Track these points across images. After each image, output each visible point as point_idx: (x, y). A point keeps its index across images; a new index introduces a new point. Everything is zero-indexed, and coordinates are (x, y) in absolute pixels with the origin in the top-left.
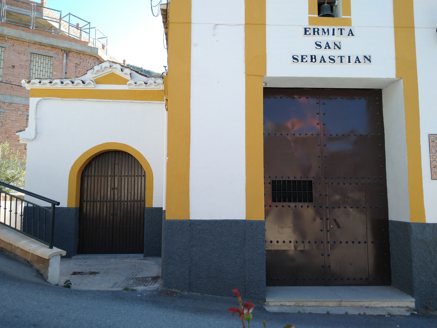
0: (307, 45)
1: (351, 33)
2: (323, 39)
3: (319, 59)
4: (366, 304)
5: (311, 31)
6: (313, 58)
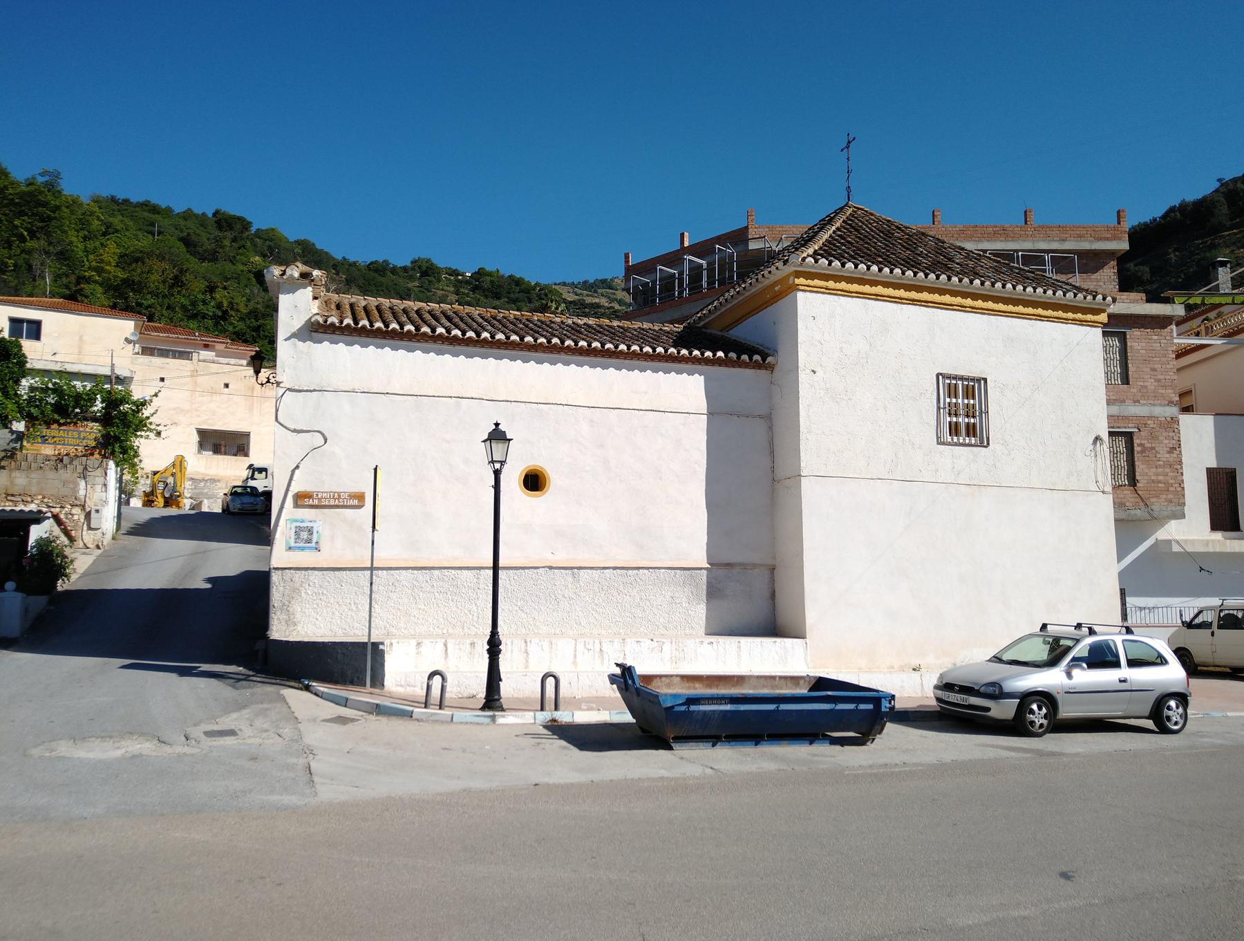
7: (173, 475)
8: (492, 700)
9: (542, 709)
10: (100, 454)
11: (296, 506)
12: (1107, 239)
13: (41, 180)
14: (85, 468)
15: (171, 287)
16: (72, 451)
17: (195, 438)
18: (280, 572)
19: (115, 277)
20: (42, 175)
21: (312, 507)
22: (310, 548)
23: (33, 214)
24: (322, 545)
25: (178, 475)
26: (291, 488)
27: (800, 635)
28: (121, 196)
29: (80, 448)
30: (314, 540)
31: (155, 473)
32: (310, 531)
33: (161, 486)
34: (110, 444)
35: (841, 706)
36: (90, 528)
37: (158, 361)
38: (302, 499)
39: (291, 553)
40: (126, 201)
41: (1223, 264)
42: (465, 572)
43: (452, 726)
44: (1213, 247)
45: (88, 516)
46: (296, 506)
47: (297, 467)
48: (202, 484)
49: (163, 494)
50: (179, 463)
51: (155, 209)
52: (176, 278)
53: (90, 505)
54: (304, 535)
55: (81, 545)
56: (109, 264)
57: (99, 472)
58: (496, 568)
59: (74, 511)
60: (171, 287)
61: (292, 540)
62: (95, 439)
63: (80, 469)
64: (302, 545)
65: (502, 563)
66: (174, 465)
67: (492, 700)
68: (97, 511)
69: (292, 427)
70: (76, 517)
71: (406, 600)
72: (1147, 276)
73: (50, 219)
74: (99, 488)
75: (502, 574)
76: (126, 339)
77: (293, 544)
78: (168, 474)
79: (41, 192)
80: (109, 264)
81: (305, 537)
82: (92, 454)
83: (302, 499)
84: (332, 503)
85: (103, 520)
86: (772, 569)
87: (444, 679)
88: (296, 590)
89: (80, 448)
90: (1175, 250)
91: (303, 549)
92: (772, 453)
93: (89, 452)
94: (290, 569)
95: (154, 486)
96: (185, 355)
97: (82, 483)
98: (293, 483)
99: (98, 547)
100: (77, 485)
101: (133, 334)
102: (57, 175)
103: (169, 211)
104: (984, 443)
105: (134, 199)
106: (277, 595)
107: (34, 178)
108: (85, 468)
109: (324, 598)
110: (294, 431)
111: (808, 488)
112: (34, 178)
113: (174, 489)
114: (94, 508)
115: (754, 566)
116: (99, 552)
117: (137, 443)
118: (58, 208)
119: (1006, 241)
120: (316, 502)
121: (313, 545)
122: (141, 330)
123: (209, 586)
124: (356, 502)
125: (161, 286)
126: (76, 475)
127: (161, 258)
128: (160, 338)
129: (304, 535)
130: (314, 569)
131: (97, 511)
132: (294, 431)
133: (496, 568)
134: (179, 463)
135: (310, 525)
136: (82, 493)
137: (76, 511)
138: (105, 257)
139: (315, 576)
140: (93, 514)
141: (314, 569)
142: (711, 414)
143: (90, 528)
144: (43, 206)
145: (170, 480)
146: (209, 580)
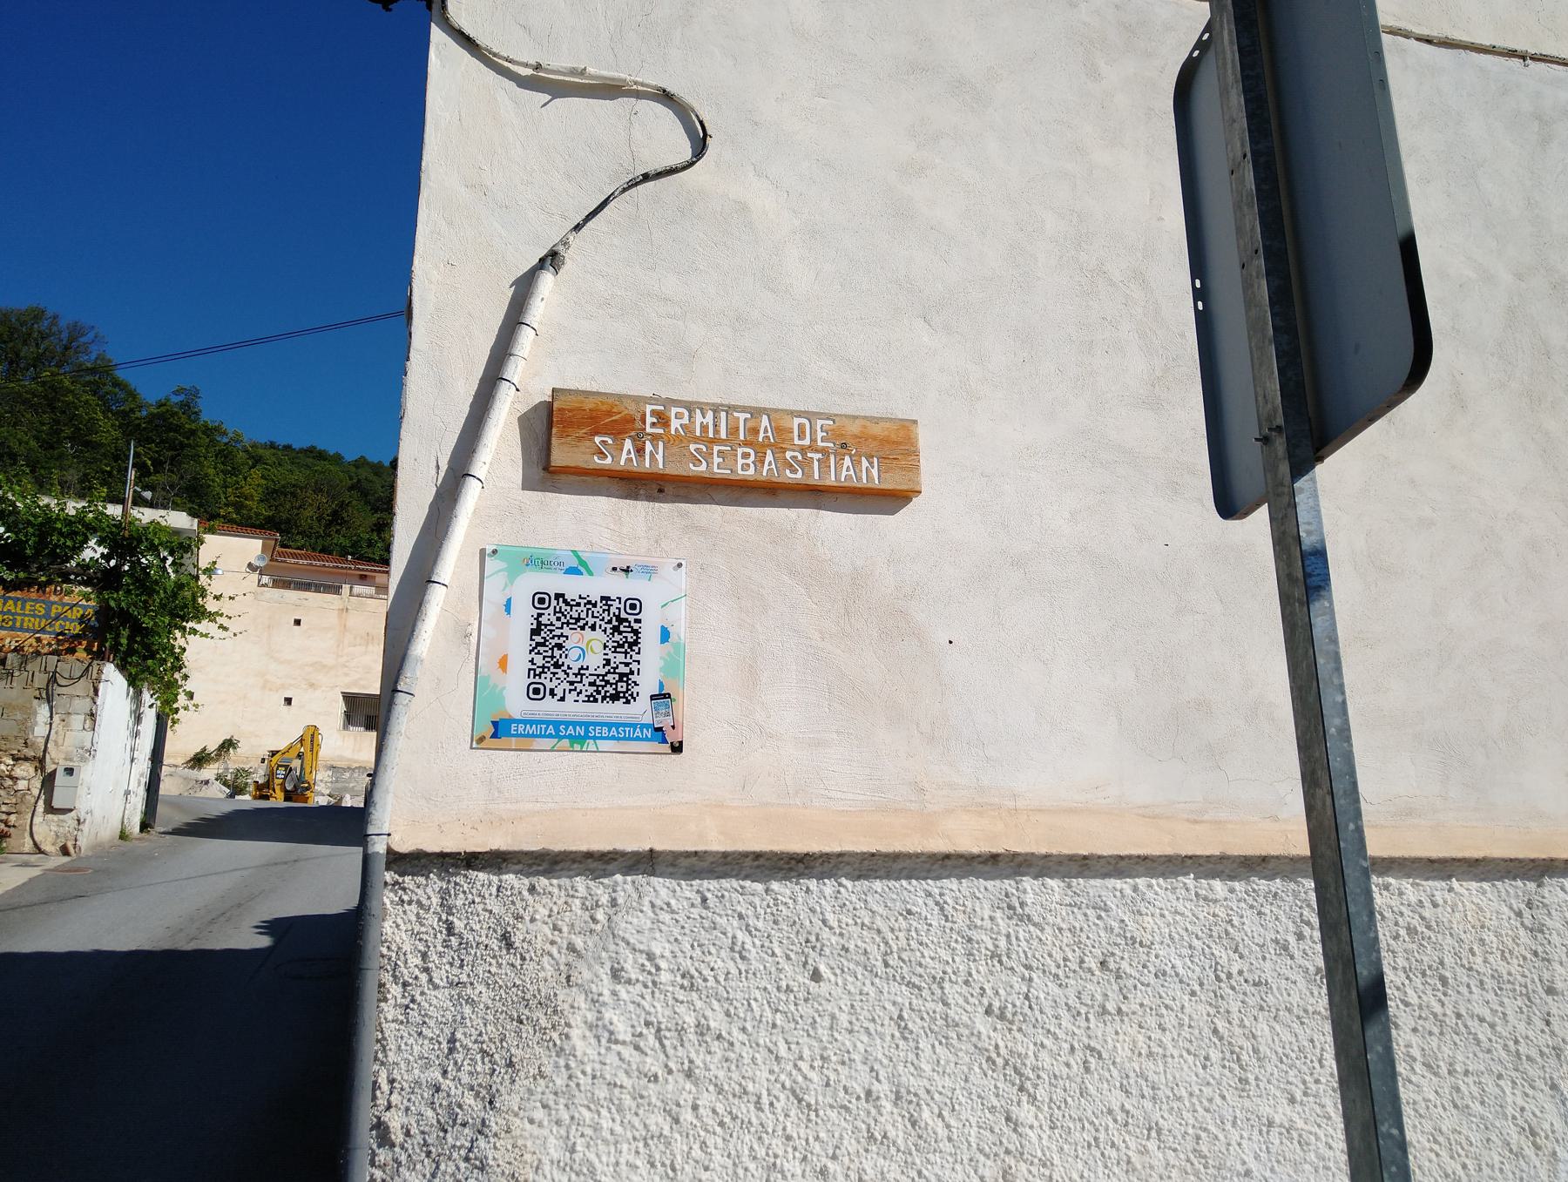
7: (300, 756)
10: (88, 650)
11: (545, 472)
13: (175, 399)
14: (53, 680)
15: (328, 525)
16: (30, 643)
17: (340, 707)
18: (429, 888)
19: (257, 514)
20: (176, 393)
21: (633, 485)
22: (621, 731)
23: (162, 441)
24: (697, 716)
25: (308, 756)
26: (515, 370)
28: (282, 441)
29: (46, 638)
30: (647, 684)
31: (274, 753)
32: (623, 625)
33: (281, 771)
34: (110, 628)
36: (50, 809)
37: (292, 595)
38: (574, 444)
39: (502, 760)
40: (288, 447)
42: (1468, 890)
45: (49, 782)
46: (545, 472)
47: (552, 259)
48: (347, 775)
49: (283, 785)
50: (310, 738)
51: (321, 456)
52: (335, 513)
53: (56, 759)
54: (588, 649)
55: (28, 845)
56: (251, 497)
57: (83, 686)
58: (1336, 864)
59: (18, 772)
60: (328, 525)
61: (516, 681)
62: (81, 620)
63: (41, 680)
64: (574, 708)
66: (302, 740)
68: (70, 771)
69: (520, 50)
70: (22, 785)
71: (1187, 1071)
73: (182, 446)
74: (77, 721)
76: (250, 565)
77: (517, 703)
78: (293, 753)
79: (174, 414)
80: (251, 497)
81: (591, 660)
82: (72, 651)
83: (574, 444)
84: (745, 467)
85: (82, 791)
88: (533, 1012)
89: (46, 638)
91: (577, 735)
93: (66, 645)
94: (496, 861)
95: (271, 775)
96: (336, 590)
97: (43, 711)
98: (525, 340)
99: (65, 851)
100: (31, 714)
101: (259, 558)
102: (195, 393)
103: (337, 459)
105: (296, 446)
106: (403, 1054)
107: (168, 400)
108: (53, 680)
109: (710, 1062)
110: (538, 82)
112: (168, 400)
113: (300, 779)
114: (64, 764)
116: (66, 859)
117: (181, 642)
118: (193, 432)
120: (656, 459)
121: (640, 711)
122: (272, 554)
123: (264, 942)
124: (870, 474)
125: (315, 524)
126: (32, 692)
127: (318, 490)
128: (300, 563)
129: (588, 649)
130: (647, 863)
131: (70, 771)
132: (538, 82)
133: (1336, 864)
134: (310, 738)
135: (620, 588)
136: (40, 731)
137: (25, 770)
138: (247, 490)
139: (654, 912)
140: (60, 778)
143: (50, 809)
144: (175, 431)
145: (296, 764)
146: (274, 927)
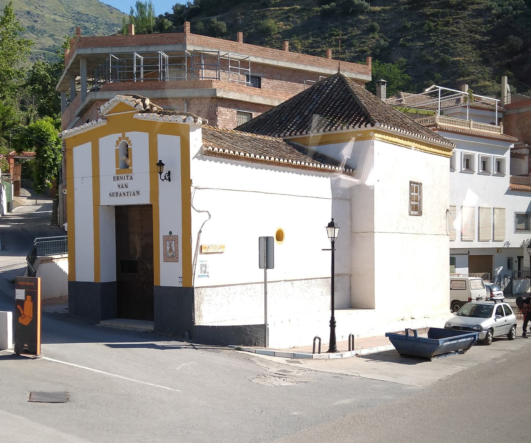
0: (113, 187)
1: (131, 178)
2: (121, 182)
3: (119, 194)
4: (131, 326)
5: (116, 179)
6: (117, 193)
8: (332, 348)
9: (349, 350)
12: (362, 73)
27: (370, 307)
35: (460, 341)
41: (383, 83)
43: (328, 361)
44: (264, 17)
47: (200, 232)
54: (204, 269)
58: (265, 282)
65: (268, 280)
67: (332, 348)
69: (198, 209)
72: (224, 30)
75: (268, 284)
86: (351, 275)
87: (320, 339)
90: (242, 14)
92: (351, 218)
104: (420, 214)
111: (378, 238)
115: (346, 274)
119: (319, 67)
121: (206, 274)
130: (207, 287)
135: (205, 263)
141: (207, 287)
142: (334, 199)
